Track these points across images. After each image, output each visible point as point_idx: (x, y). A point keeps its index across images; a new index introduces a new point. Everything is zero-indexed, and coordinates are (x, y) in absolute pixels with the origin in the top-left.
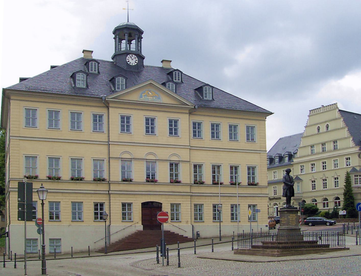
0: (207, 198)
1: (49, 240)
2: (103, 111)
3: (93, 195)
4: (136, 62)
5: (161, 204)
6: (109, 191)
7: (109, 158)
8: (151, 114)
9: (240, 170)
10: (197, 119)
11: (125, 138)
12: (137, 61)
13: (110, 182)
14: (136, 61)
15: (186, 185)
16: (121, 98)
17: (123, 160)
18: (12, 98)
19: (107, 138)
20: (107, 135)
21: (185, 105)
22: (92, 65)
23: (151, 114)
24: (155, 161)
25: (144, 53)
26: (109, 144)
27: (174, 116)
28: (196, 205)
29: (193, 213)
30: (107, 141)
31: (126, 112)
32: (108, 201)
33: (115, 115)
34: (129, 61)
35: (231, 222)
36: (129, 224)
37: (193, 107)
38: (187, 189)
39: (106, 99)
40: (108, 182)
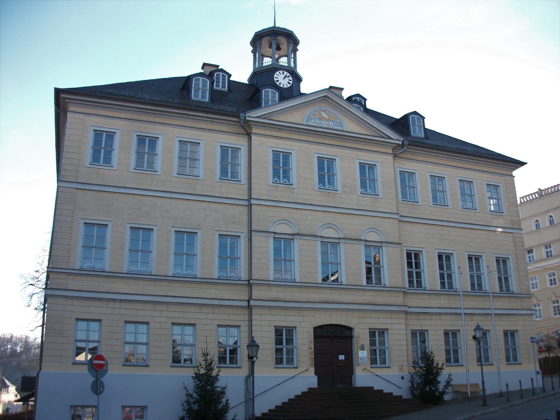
0: (434, 317)
1: (120, 407)
2: (240, 142)
3: (217, 310)
4: (290, 84)
5: (350, 329)
6: (249, 301)
7: (250, 231)
8: (327, 152)
9: (484, 263)
10: (408, 166)
11: (281, 193)
12: (291, 82)
13: (251, 282)
14: (290, 82)
15: (393, 290)
16: (280, 119)
17: (278, 238)
18: (71, 108)
19: (246, 192)
20: (246, 187)
21: (383, 137)
22: (218, 78)
23: (327, 152)
24: (291, 237)
25: (300, 71)
26: (251, 205)
27: (368, 158)
28: (414, 333)
29: (410, 347)
30: (247, 199)
31: (283, 146)
32: (247, 323)
33: (264, 146)
34: (278, 81)
35: (507, 364)
36: (291, 373)
37: (401, 143)
38: (399, 299)
39: (248, 118)
40: (247, 283)
